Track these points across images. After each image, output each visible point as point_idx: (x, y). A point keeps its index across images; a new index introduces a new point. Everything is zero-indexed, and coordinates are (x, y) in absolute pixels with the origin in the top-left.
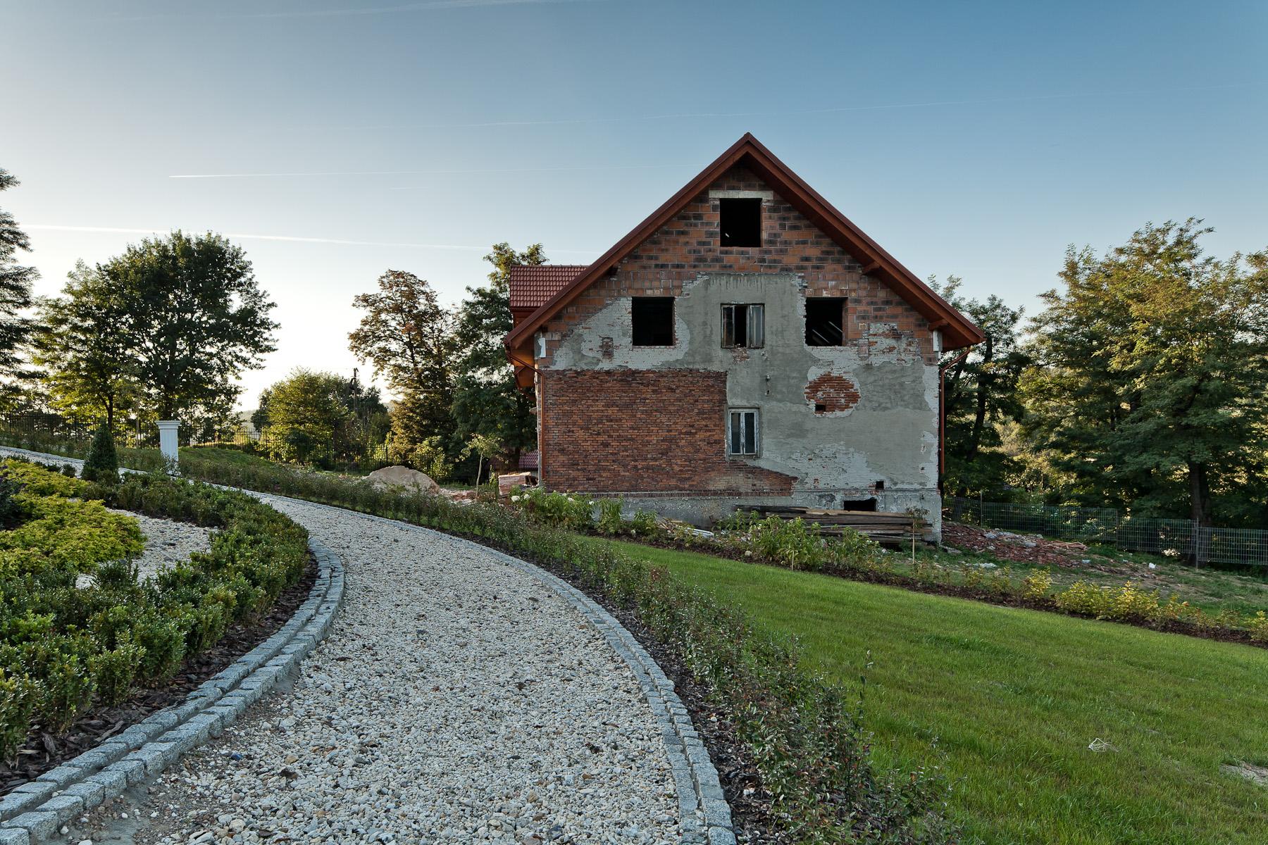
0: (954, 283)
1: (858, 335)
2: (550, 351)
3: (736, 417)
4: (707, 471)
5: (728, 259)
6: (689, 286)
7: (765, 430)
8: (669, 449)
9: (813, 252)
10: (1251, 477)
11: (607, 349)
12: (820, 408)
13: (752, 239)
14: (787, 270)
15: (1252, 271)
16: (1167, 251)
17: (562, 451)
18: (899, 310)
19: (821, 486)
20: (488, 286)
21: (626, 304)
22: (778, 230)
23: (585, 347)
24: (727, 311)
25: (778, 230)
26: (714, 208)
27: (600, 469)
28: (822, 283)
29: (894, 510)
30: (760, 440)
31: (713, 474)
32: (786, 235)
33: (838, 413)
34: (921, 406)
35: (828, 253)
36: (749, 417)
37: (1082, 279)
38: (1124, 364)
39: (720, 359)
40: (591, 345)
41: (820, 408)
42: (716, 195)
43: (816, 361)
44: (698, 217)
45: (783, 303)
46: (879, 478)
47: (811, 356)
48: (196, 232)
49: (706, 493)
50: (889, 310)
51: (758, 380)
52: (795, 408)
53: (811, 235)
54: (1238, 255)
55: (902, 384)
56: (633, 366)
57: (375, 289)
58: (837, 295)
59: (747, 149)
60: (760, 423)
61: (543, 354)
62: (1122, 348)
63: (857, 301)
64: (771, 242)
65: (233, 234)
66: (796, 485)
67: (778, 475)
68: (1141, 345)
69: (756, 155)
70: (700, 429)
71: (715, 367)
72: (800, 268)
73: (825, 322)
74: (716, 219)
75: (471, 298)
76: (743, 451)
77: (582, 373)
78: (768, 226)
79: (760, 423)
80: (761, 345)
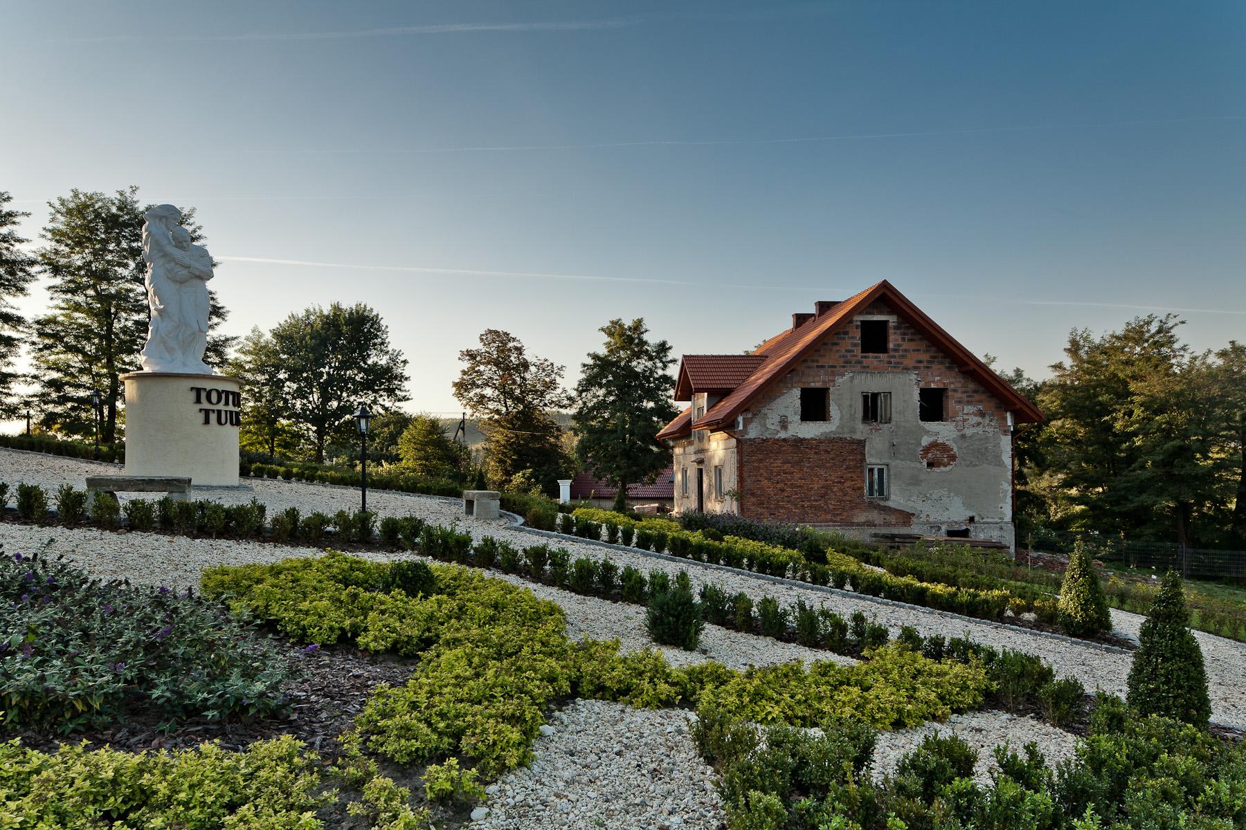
0: (1019, 373)
1: (956, 414)
2: (745, 426)
3: (871, 470)
4: (852, 508)
5: (866, 362)
6: (839, 380)
7: (892, 481)
8: (826, 494)
9: (925, 357)
10: (1217, 509)
11: (784, 424)
12: (930, 465)
13: (883, 348)
14: (907, 369)
15: (1220, 362)
16: (1150, 343)
17: (753, 494)
18: (984, 397)
19: (931, 520)
20: (603, 351)
21: (797, 392)
22: (900, 342)
23: (769, 423)
24: (865, 398)
25: (900, 342)
26: (857, 327)
27: (778, 507)
28: (930, 378)
29: (982, 537)
30: (889, 487)
31: (856, 511)
32: (906, 345)
33: (943, 469)
34: (1000, 463)
35: (934, 357)
36: (881, 471)
37: (1082, 353)
38: (1126, 426)
39: (861, 430)
40: (772, 421)
41: (930, 465)
42: (858, 318)
43: (927, 432)
44: (847, 333)
45: (904, 391)
46: (971, 514)
47: (923, 429)
48: (348, 304)
49: (852, 524)
50: (977, 397)
51: (887, 445)
52: (913, 465)
53: (923, 345)
54: (1210, 351)
55: (986, 449)
56: (801, 436)
57: (477, 346)
58: (941, 386)
59: (884, 290)
60: (889, 475)
61: (741, 428)
62: (1125, 414)
63: (955, 391)
64: (895, 350)
65: (377, 305)
66: (914, 519)
67: (901, 512)
68: (1138, 412)
69: (889, 294)
70: (847, 480)
71: (858, 436)
72: (915, 368)
73: (933, 405)
74: (858, 334)
75: (590, 362)
76: (876, 495)
77: (766, 440)
78: (894, 339)
79: (889, 475)
80: (889, 421)
